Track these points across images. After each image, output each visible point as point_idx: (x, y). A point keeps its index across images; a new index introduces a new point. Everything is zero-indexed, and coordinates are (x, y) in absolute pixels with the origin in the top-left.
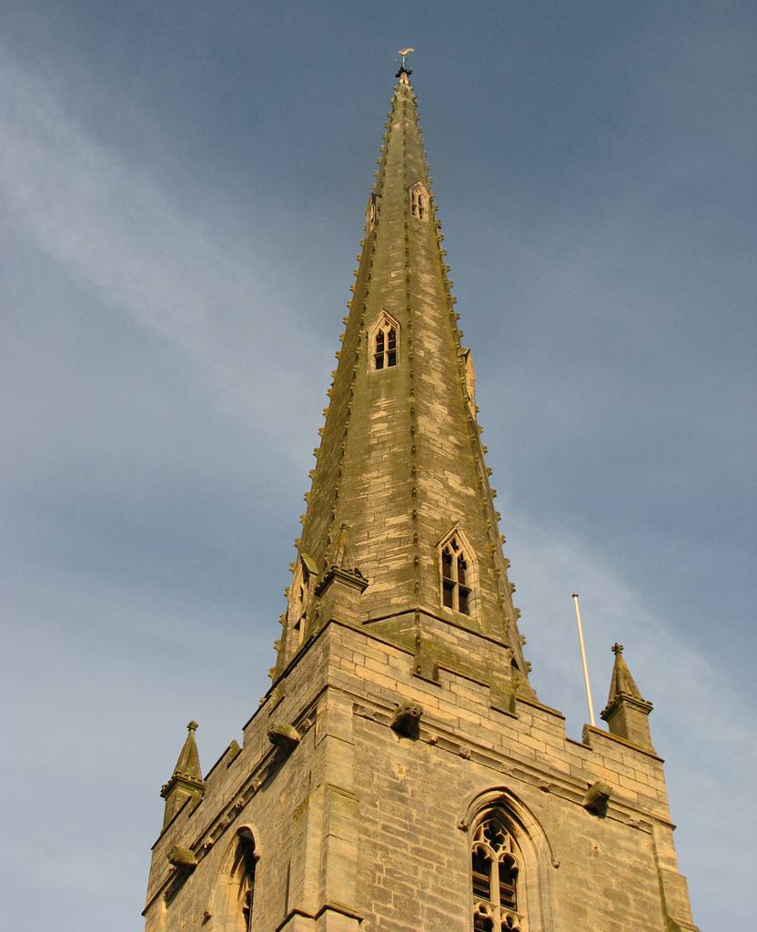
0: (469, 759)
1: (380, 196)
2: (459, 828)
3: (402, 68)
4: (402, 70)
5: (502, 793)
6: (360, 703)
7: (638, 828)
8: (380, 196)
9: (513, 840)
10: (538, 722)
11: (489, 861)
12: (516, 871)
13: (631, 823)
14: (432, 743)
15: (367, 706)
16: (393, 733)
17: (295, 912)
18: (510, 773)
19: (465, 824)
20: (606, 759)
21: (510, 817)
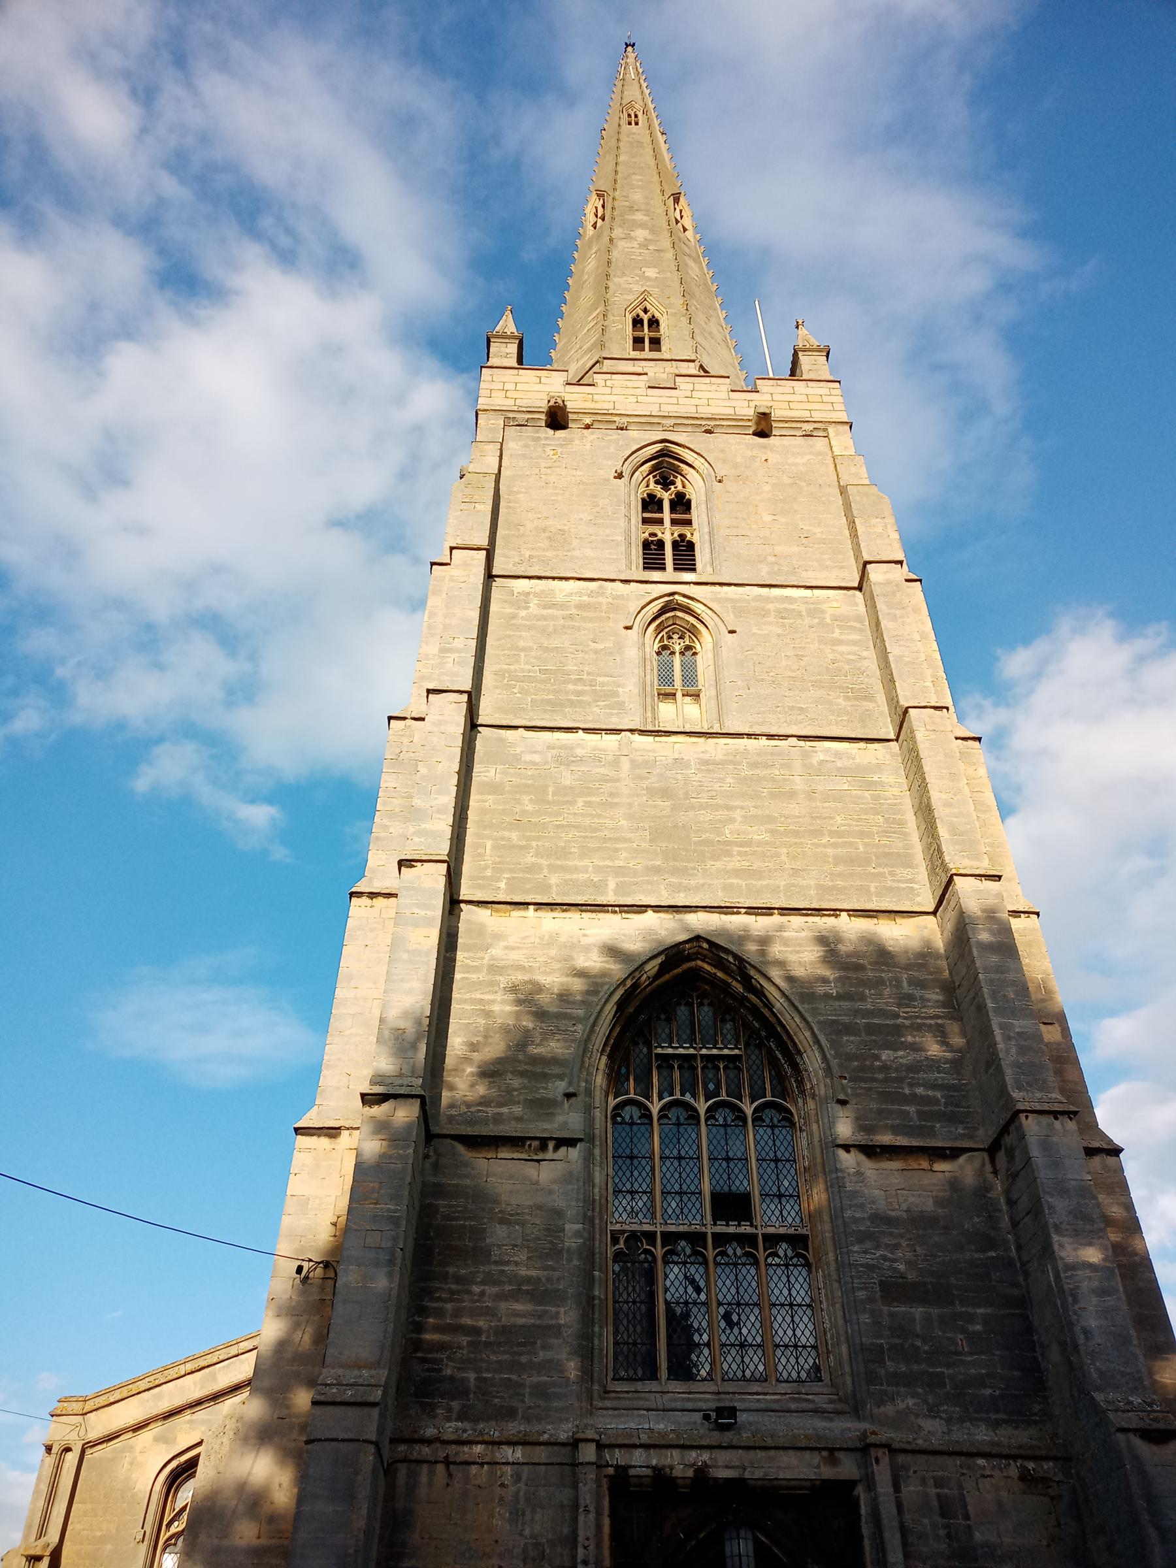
0: (626, 430)
1: (605, 130)
2: (615, 477)
3: (626, 44)
4: (627, 45)
5: (663, 444)
6: (511, 415)
7: (812, 436)
8: (605, 130)
9: (684, 479)
10: (697, 387)
11: (661, 501)
12: (689, 501)
13: (804, 433)
14: (588, 427)
15: (518, 416)
16: (548, 429)
17: (952, 875)
18: (671, 428)
19: (619, 471)
20: (832, 430)
21: (671, 461)
